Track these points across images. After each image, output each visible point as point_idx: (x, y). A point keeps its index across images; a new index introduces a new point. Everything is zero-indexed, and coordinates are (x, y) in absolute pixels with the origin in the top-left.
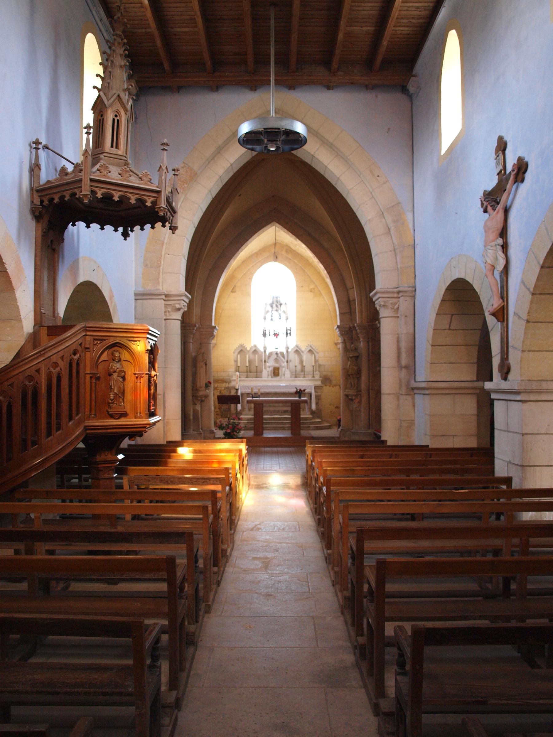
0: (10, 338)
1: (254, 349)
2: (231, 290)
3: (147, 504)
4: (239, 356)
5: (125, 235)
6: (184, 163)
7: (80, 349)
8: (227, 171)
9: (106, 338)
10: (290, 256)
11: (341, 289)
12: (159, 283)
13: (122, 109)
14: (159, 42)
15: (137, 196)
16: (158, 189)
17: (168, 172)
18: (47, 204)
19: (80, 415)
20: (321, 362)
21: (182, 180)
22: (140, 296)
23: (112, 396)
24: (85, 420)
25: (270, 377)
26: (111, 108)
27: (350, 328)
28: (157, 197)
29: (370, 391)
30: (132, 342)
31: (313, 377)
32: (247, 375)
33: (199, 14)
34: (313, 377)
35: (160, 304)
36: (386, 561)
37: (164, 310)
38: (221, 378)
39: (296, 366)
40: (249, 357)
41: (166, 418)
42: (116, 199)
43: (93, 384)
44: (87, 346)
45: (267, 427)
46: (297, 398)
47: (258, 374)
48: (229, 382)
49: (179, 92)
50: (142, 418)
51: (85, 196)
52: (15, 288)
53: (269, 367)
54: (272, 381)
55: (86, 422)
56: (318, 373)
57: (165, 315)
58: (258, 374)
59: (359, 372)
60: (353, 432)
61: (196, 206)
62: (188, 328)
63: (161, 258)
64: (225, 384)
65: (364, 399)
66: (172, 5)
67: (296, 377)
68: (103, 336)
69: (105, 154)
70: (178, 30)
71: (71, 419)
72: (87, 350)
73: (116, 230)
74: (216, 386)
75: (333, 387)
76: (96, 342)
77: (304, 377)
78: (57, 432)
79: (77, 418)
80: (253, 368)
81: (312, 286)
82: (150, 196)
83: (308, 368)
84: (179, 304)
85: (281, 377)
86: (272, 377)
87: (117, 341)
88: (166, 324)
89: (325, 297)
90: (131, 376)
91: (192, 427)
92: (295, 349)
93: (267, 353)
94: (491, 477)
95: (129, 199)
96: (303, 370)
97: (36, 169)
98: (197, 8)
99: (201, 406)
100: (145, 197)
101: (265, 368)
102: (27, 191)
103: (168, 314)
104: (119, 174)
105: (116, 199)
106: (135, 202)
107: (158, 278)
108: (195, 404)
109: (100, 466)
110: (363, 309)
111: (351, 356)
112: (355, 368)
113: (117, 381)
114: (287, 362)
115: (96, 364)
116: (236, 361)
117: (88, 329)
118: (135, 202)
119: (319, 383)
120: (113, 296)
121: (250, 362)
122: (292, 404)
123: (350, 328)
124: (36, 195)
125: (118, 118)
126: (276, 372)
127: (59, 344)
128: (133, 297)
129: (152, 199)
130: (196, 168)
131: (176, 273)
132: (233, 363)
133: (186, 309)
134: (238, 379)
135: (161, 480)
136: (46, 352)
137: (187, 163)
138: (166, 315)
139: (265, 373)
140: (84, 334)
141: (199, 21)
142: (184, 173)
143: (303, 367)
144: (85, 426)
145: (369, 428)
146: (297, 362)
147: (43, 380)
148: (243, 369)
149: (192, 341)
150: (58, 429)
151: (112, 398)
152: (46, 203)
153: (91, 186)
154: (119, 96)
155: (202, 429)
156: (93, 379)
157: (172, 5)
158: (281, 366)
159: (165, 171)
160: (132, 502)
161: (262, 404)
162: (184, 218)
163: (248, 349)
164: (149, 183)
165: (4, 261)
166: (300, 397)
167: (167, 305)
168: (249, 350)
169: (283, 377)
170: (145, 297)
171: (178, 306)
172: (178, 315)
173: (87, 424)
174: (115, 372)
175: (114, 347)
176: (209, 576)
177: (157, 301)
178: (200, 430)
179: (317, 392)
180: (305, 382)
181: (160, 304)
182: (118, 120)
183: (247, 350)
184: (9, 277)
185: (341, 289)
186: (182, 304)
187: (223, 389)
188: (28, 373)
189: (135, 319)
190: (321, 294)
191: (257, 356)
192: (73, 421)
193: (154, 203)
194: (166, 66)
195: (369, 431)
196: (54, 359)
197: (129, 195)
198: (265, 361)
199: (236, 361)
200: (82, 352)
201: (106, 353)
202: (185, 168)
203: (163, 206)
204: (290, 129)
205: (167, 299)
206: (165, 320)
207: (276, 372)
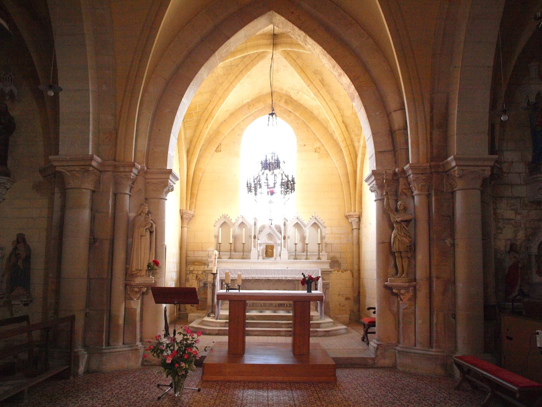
1: (240, 221)
2: (215, 149)
4: (220, 229)
10: (290, 108)
11: (378, 113)
20: (326, 240)
25: (261, 258)
27: (395, 174)
29: (434, 280)
31: (319, 258)
32: (230, 255)
34: (319, 258)
38: (200, 258)
39: (296, 244)
40: (234, 232)
45: (254, 331)
46: (305, 292)
47: (245, 254)
48: (206, 264)
53: (260, 245)
54: (264, 263)
56: (324, 253)
58: (245, 254)
59: (412, 248)
60: (399, 351)
64: (203, 266)
65: (422, 294)
67: (296, 259)
74: (192, 268)
75: (342, 272)
77: (307, 259)
80: (239, 247)
81: (317, 145)
83: (313, 247)
85: (276, 259)
86: (263, 259)
89: (333, 159)
92: (295, 222)
93: (259, 226)
94: (312, 289)
96: (305, 250)
99: (142, 304)
101: (255, 247)
108: (128, 298)
110: (421, 140)
111: (399, 220)
112: (406, 240)
114: (284, 238)
116: (217, 237)
119: (327, 267)
121: (235, 238)
122: (295, 302)
123: (395, 174)
126: (269, 252)
132: (213, 240)
134: (217, 260)
139: (254, 253)
143: (305, 245)
145: (431, 345)
146: (297, 240)
148: (225, 247)
149: (128, 192)
155: (141, 340)
158: (276, 243)
161: (245, 301)
163: (233, 221)
166: (309, 290)
168: (235, 223)
169: (278, 258)
179: (324, 280)
180: (309, 265)
183: (232, 223)
185: (378, 113)
187: (200, 272)
190: (328, 155)
191: (244, 229)
195: (433, 352)
198: (255, 237)
199: (217, 237)
207: (269, 252)
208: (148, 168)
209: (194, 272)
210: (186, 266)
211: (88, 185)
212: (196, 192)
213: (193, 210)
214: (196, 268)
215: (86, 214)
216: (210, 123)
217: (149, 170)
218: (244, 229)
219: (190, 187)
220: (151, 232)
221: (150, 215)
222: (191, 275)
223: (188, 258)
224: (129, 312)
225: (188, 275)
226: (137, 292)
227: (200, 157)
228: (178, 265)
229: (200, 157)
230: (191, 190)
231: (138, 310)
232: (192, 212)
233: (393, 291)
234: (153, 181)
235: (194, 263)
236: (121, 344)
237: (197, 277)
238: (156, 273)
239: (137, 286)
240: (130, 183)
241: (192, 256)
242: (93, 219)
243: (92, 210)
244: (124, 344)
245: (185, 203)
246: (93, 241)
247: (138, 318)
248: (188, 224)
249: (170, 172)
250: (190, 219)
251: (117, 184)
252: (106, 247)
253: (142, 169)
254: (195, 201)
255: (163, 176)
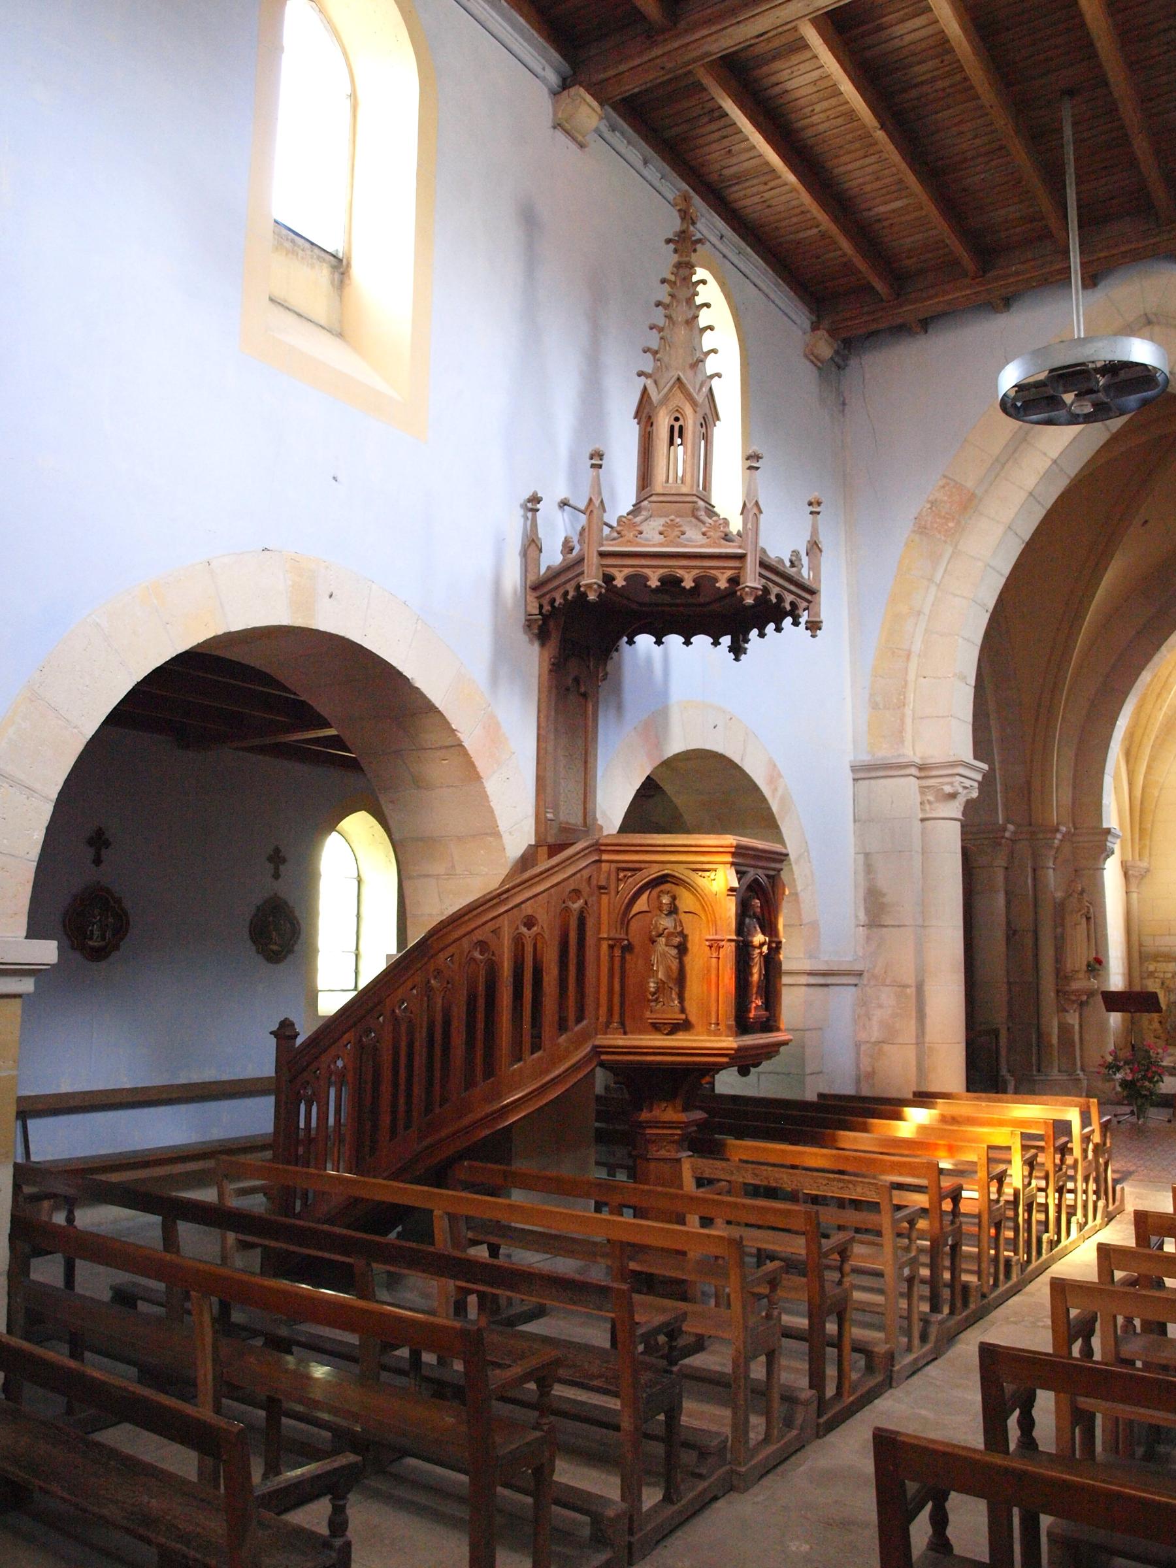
0: (486, 869)
3: (628, 1218)
5: (737, 650)
6: (945, 476)
7: (585, 890)
8: (1047, 476)
9: (643, 865)
12: (902, 742)
13: (688, 404)
14: (845, 245)
15: (697, 571)
16: (740, 551)
17: (761, 512)
18: (548, 611)
19: (585, 1022)
21: (943, 514)
22: (864, 772)
23: (652, 985)
24: (596, 1034)
26: (664, 407)
28: (740, 568)
30: (700, 873)
33: (903, 166)
35: (908, 788)
36: (894, 1439)
37: (919, 800)
41: (928, 1039)
42: (688, 584)
43: (617, 960)
44: (603, 883)
49: (926, 332)
50: (720, 1035)
51: (589, 586)
52: (481, 774)
55: (599, 1036)
57: (922, 810)
61: (980, 564)
62: (1041, 836)
63: (905, 686)
66: (850, 167)
68: (640, 862)
69: (654, 498)
70: (882, 209)
71: (562, 1026)
72: (602, 891)
73: (716, 643)
74: (1151, 968)
76: (621, 875)
78: (532, 1053)
79: (577, 1029)
82: (725, 568)
84: (951, 784)
87: (666, 872)
88: (924, 829)
90: (700, 945)
91: (1056, 1064)
95: (647, 579)
97: (531, 549)
98: (895, 157)
99: (1081, 1015)
100: (712, 571)
102: (515, 593)
103: (927, 807)
104: (661, 533)
105: (688, 584)
106: (727, 585)
107: (901, 730)
109: (648, 1131)
113: (664, 955)
115: (625, 919)
117: (603, 848)
118: (727, 585)
120: (780, 776)
124: (531, 597)
125: (681, 422)
127: (538, 879)
128: (849, 775)
129: (729, 573)
130: (970, 484)
131: (943, 717)
133: (975, 794)
135: (754, 1174)
136: (512, 896)
137: (951, 476)
138: (922, 810)
140: (597, 858)
141: (911, 179)
142: (946, 498)
144: (595, 1047)
147: (506, 950)
149: (1051, 864)
150: (535, 1047)
151: (652, 990)
152: (547, 608)
153: (603, 566)
154: (679, 379)
155: (1083, 1070)
156: (616, 950)
157: (850, 167)
159: (755, 510)
160: (598, 1209)
162: (955, 595)
164: (723, 542)
165: (454, 727)
167: (924, 787)
170: (873, 774)
171: (948, 789)
172: (955, 809)
173: (597, 1043)
174: (660, 935)
175: (662, 883)
176: (742, 1403)
177: (902, 780)
178: (1079, 1072)
181: (908, 788)
182: (681, 428)
184: (468, 754)
186: (956, 784)
187: (1170, 975)
188: (478, 936)
189: (855, 821)
192: (569, 1034)
193: (734, 581)
194: (879, 285)
196: (528, 909)
197: (646, 571)
200: (592, 895)
201: (644, 897)
202: (947, 488)
203: (749, 584)
204: (1125, 359)
205: (923, 774)
206: (922, 820)
208: (1076, 828)
209: (1156, 974)
210: (1141, 964)
211: (1001, 861)
212: (1149, 825)
213: (1146, 859)
214: (1162, 966)
215: (1001, 900)
216: (1165, 701)
217: (1077, 831)
218: (964, 1248)
219: (1137, 819)
220: (1088, 919)
221: (1085, 895)
222: (1152, 980)
223: (1143, 949)
224: (1065, 1029)
225: (1145, 982)
226: (1073, 1002)
227: (1153, 759)
228: (1126, 961)
229: (1153, 759)
230: (1140, 824)
231: (1077, 1027)
232: (1145, 864)
233: (744, 920)
234: (1086, 845)
235: (1157, 957)
236: (1055, 1071)
237: (1163, 983)
238: (1099, 975)
239: (1074, 992)
240: (1053, 852)
241: (1151, 945)
242: (1008, 903)
243: (1007, 893)
244: (1059, 1071)
245: (1130, 850)
246: (1012, 933)
247: (1077, 1037)
248: (1138, 887)
249: (1108, 831)
250: (1143, 877)
251: (1035, 856)
252: (1029, 941)
253: (1068, 833)
254: (1148, 843)
255: (1097, 838)
